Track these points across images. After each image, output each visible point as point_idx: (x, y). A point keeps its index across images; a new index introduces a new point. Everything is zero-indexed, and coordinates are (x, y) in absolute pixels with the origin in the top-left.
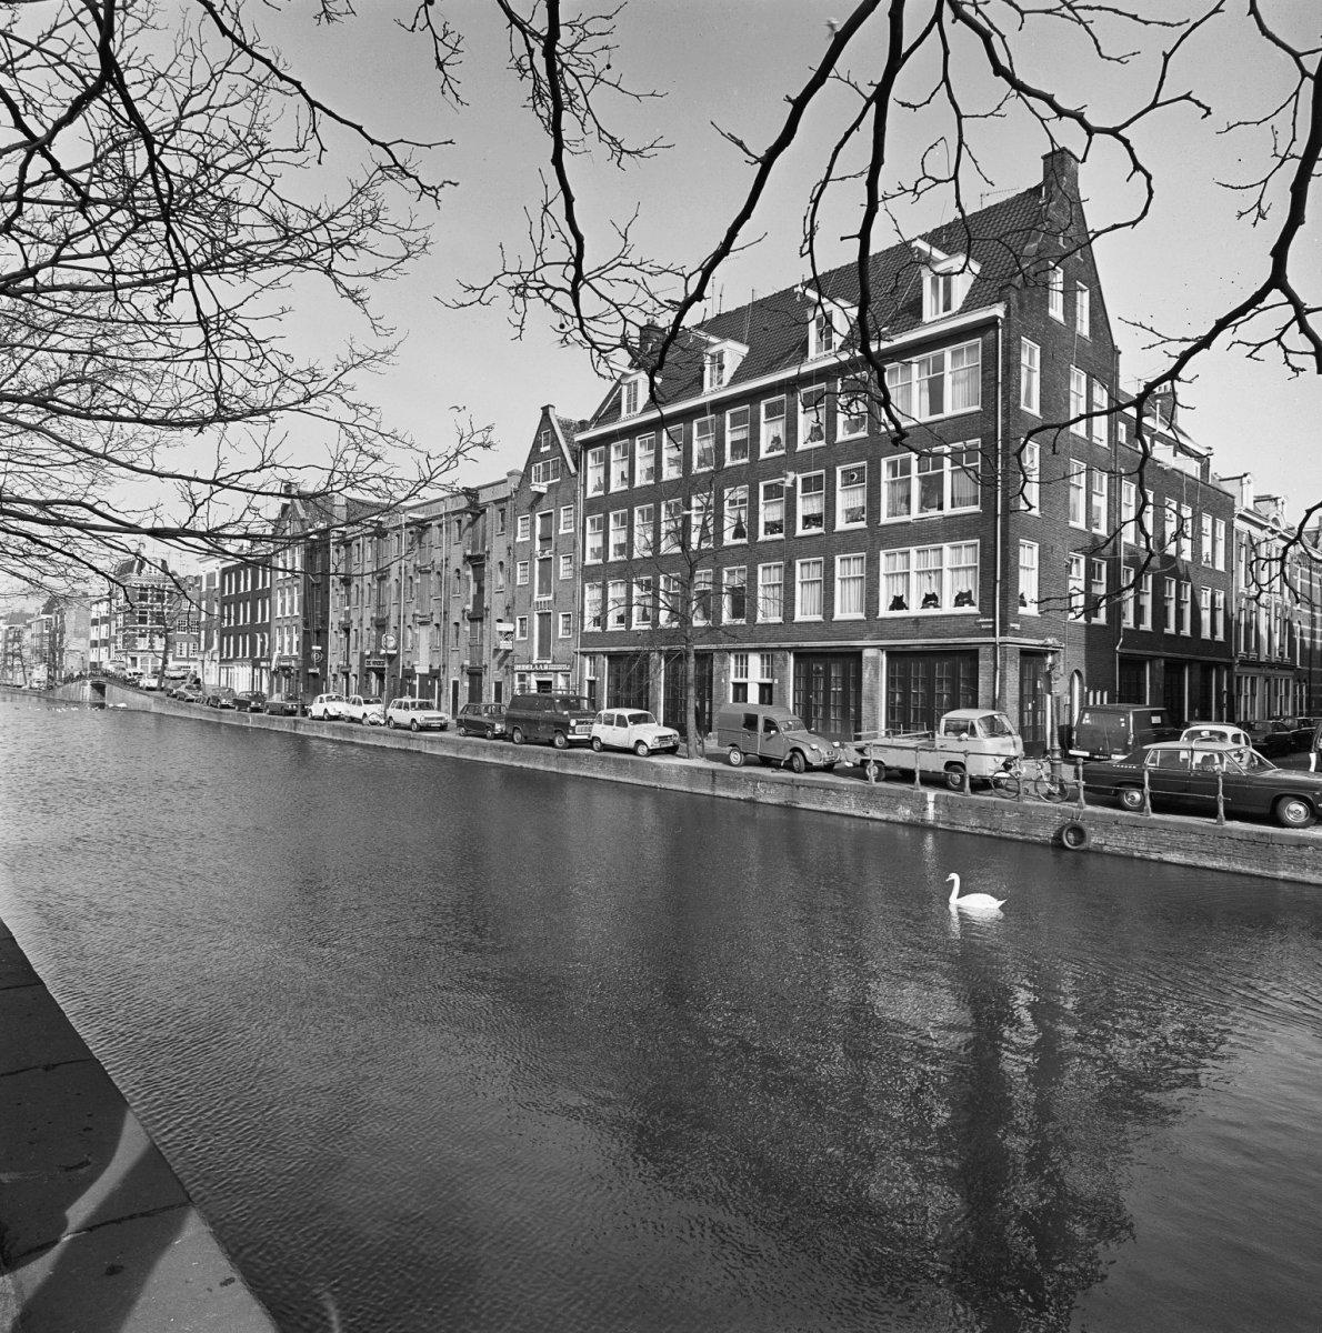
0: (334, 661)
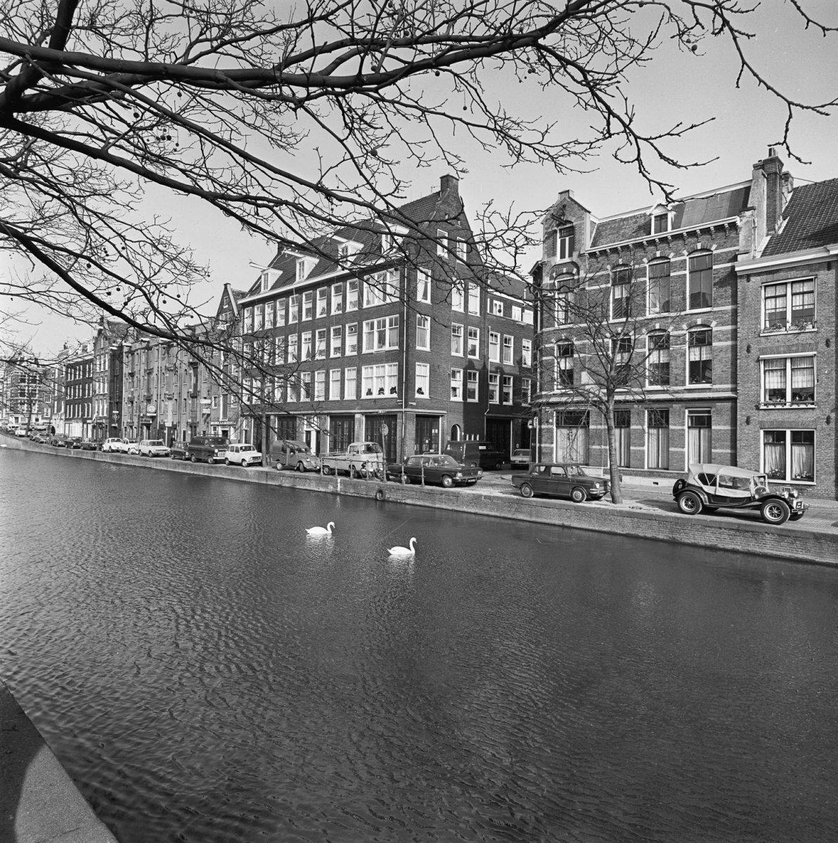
0: (126, 419)
